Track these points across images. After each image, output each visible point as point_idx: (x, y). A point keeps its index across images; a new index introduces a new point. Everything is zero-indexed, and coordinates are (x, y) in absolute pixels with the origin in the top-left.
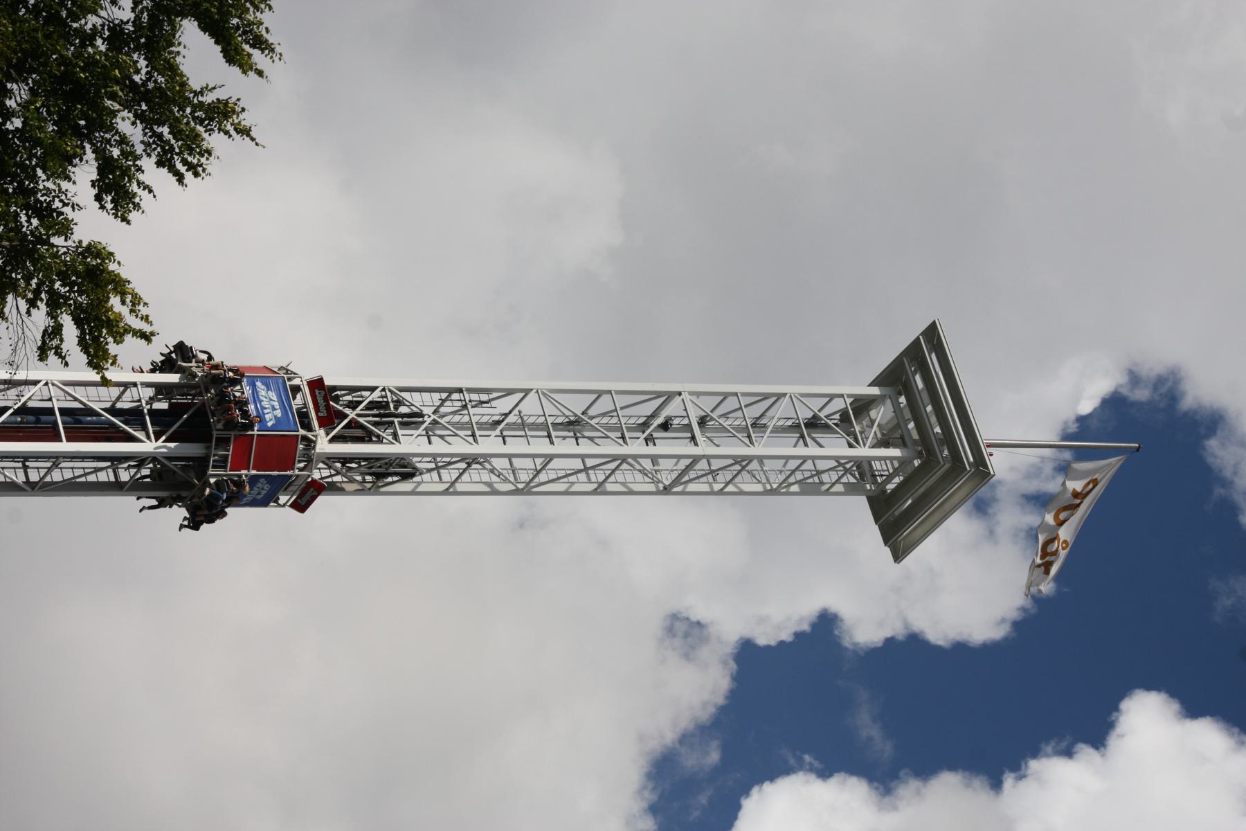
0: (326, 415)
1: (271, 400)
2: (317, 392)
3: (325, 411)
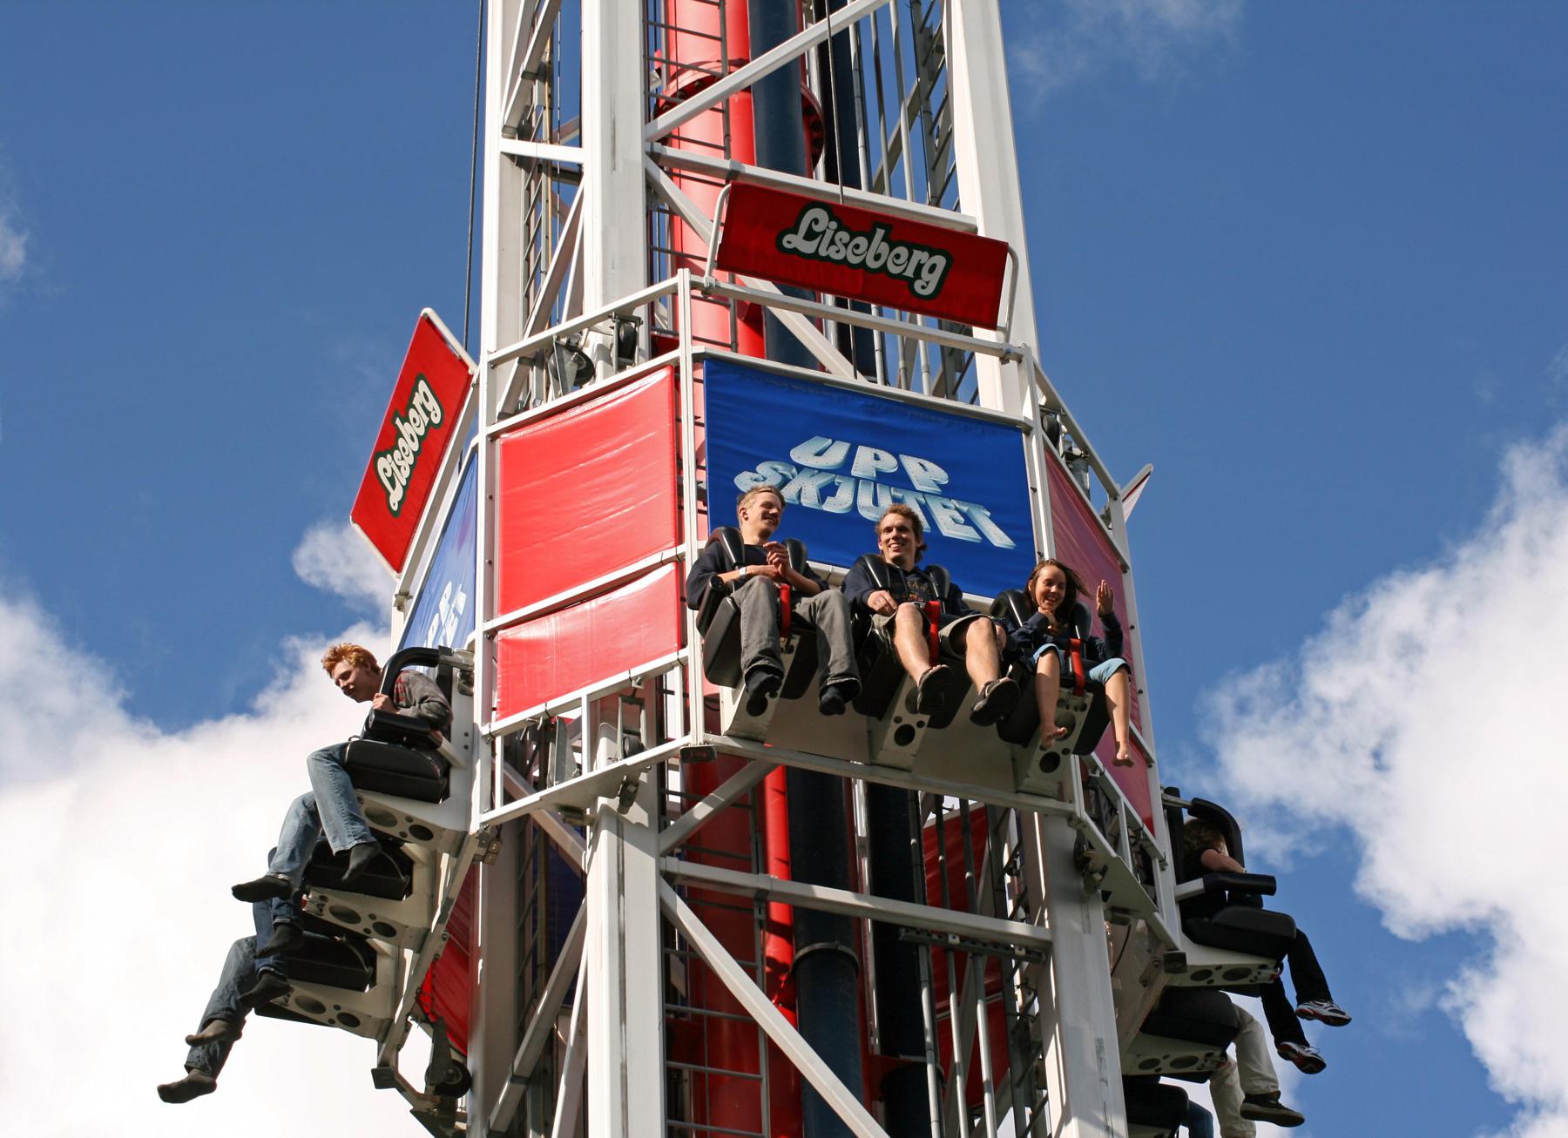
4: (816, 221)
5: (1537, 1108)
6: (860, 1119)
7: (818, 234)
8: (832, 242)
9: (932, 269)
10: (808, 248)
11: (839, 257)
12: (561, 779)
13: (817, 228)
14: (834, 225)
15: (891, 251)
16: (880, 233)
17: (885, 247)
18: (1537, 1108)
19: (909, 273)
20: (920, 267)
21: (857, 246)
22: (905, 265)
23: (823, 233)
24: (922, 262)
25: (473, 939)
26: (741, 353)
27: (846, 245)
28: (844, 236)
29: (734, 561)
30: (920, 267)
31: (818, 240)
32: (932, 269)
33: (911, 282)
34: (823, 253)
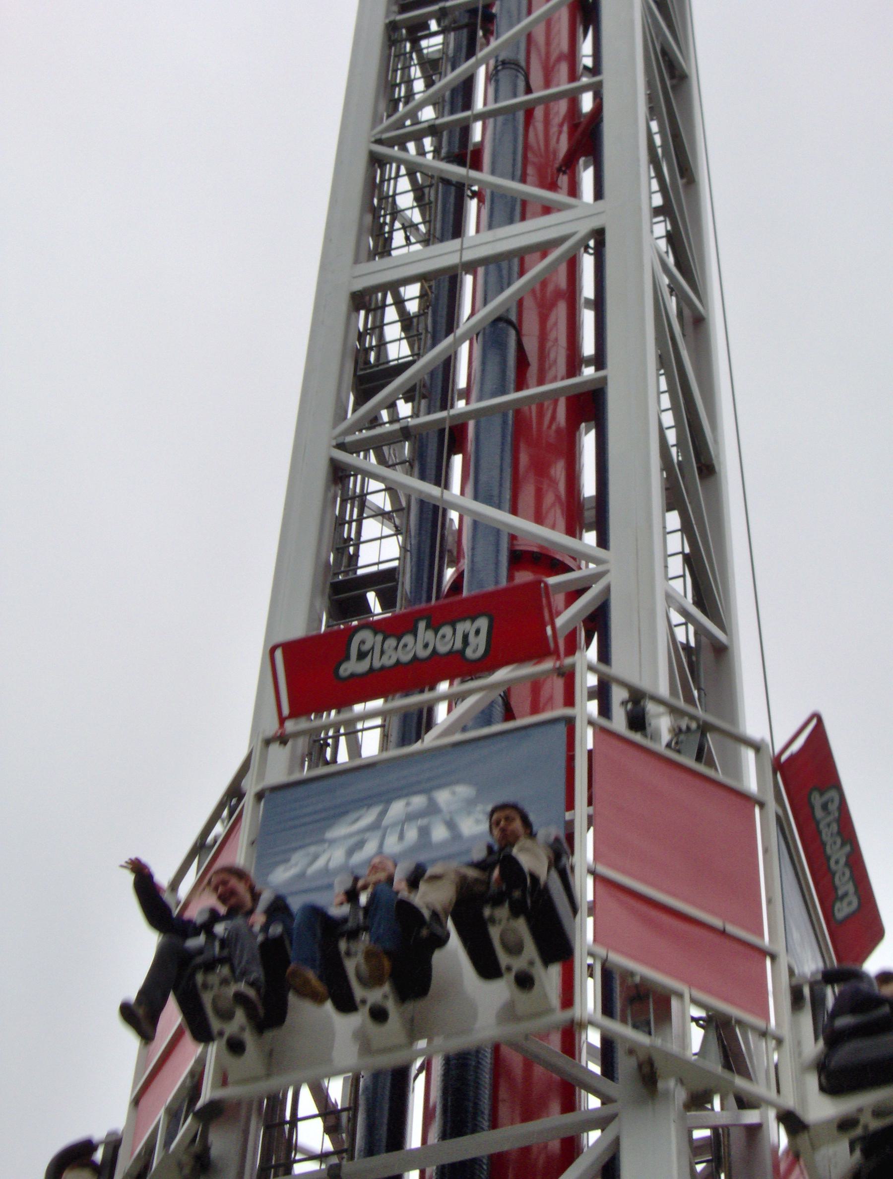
0: (483, 623)
1: (375, 826)
2: (352, 667)
3: (463, 627)
4: (363, 642)
5: (472, 625)
6: (439, 560)
7: (369, 652)
8: (382, 652)
9: (477, 632)
10: (362, 667)
11: (393, 661)
12: (541, 382)
13: (366, 647)
14: (380, 638)
15: (436, 634)
16: (422, 625)
17: (430, 635)
18: (472, 625)
19: (458, 645)
20: (465, 637)
21: (405, 646)
22: (453, 640)
23: (373, 648)
24: (466, 632)
25: (579, 267)
26: (526, 518)
27: (396, 648)
28: (391, 642)
29: (273, 1170)
30: (465, 637)
31: (370, 653)
32: (477, 632)
33: (462, 652)
34: (377, 664)
